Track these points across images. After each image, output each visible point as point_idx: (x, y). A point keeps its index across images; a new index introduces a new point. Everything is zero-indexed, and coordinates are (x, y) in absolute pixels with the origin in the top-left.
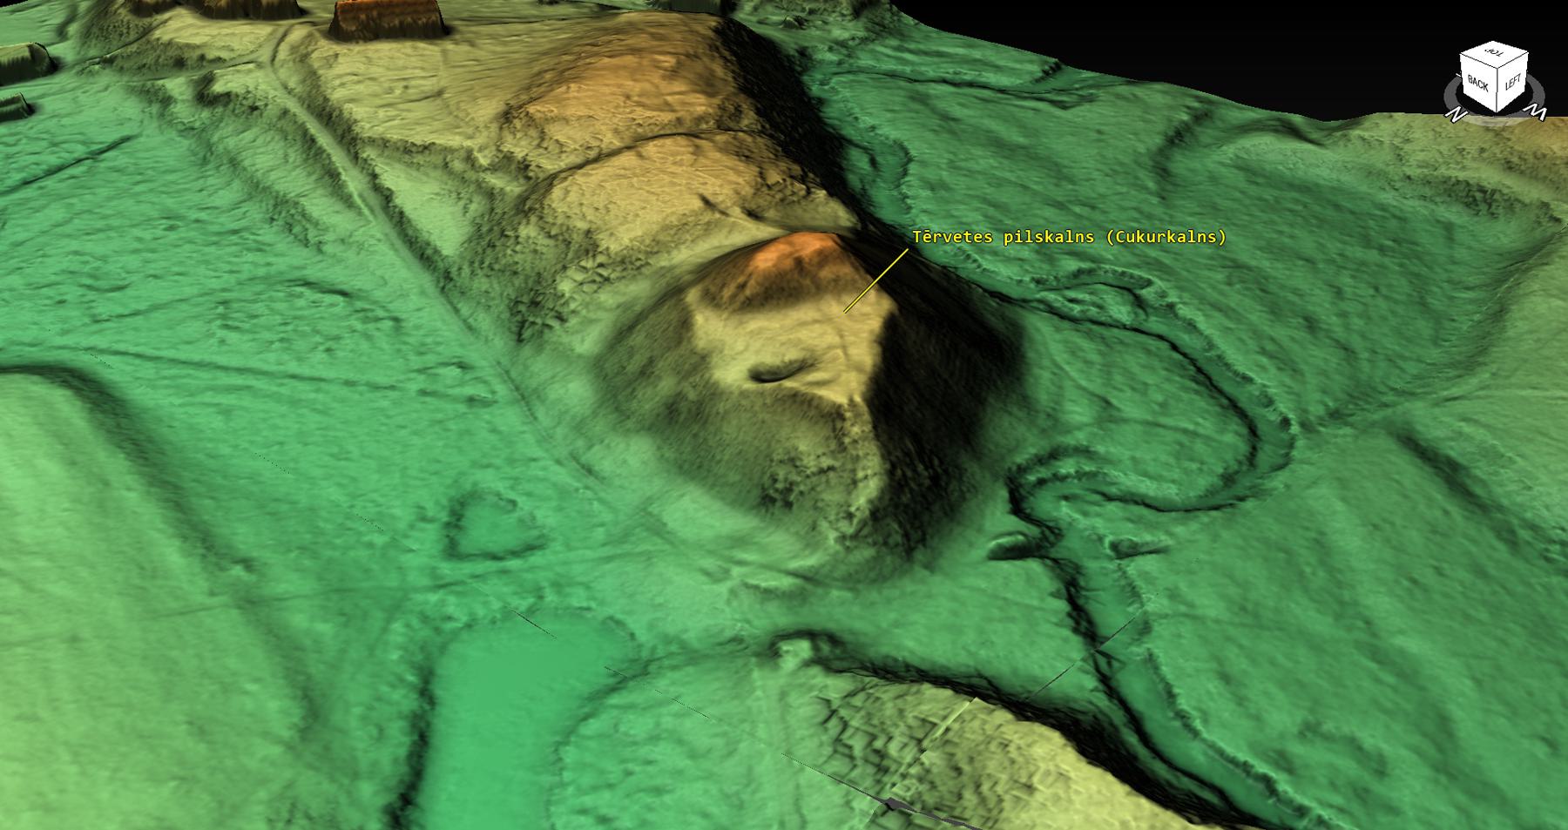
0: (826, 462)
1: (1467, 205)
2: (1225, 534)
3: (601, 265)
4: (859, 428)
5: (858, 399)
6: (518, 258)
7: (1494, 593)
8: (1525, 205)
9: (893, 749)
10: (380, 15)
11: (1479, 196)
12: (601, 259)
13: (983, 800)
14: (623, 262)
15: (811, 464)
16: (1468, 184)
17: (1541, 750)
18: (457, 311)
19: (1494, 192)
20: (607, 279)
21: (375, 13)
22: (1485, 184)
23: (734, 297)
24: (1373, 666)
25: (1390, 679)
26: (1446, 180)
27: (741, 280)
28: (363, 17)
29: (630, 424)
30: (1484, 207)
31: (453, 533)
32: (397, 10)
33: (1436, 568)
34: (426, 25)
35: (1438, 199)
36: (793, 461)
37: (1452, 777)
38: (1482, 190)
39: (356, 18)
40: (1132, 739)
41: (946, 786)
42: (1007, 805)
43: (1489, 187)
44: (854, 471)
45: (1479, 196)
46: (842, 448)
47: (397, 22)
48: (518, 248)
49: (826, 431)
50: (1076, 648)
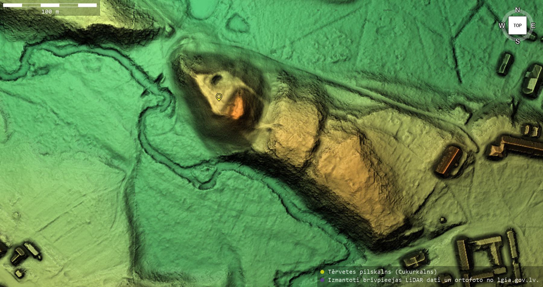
0: (193, 66)
1: (160, 275)
2: (135, 107)
3: (283, 94)
4: (191, 73)
5: (196, 78)
6: (306, 89)
7: (92, 122)
8: (146, 278)
9: (139, 17)
10: (448, 157)
11: (159, 279)
12: (284, 95)
13: (120, 12)
14: (280, 97)
15: (196, 65)
16: (162, 281)
17: (71, 88)
18: (307, 72)
19: (155, 281)
20: (279, 92)
21: (449, 156)
22: (158, 282)
23: (240, 91)
24: (99, 90)
25: (96, 88)
26: (168, 281)
27: (241, 94)
28: (451, 153)
29: (238, 60)
30: (156, 276)
31: (242, 19)
32: (446, 162)
33: (102, 122)
34: (437, 166)
35: (168, 275)
36: (199, 63)
37: (79, 73)
38: (158, 281)
39: (451, 151)
40: (116, 47)
41: (127, 13)
42: (116, 13)
43: (157, 282)
44: (187, 66)
45: (159, 279)
46: (192, 69)
47: (443, 160)
48: (309, 92)
49: (197, 70)
50: (138, 62)
